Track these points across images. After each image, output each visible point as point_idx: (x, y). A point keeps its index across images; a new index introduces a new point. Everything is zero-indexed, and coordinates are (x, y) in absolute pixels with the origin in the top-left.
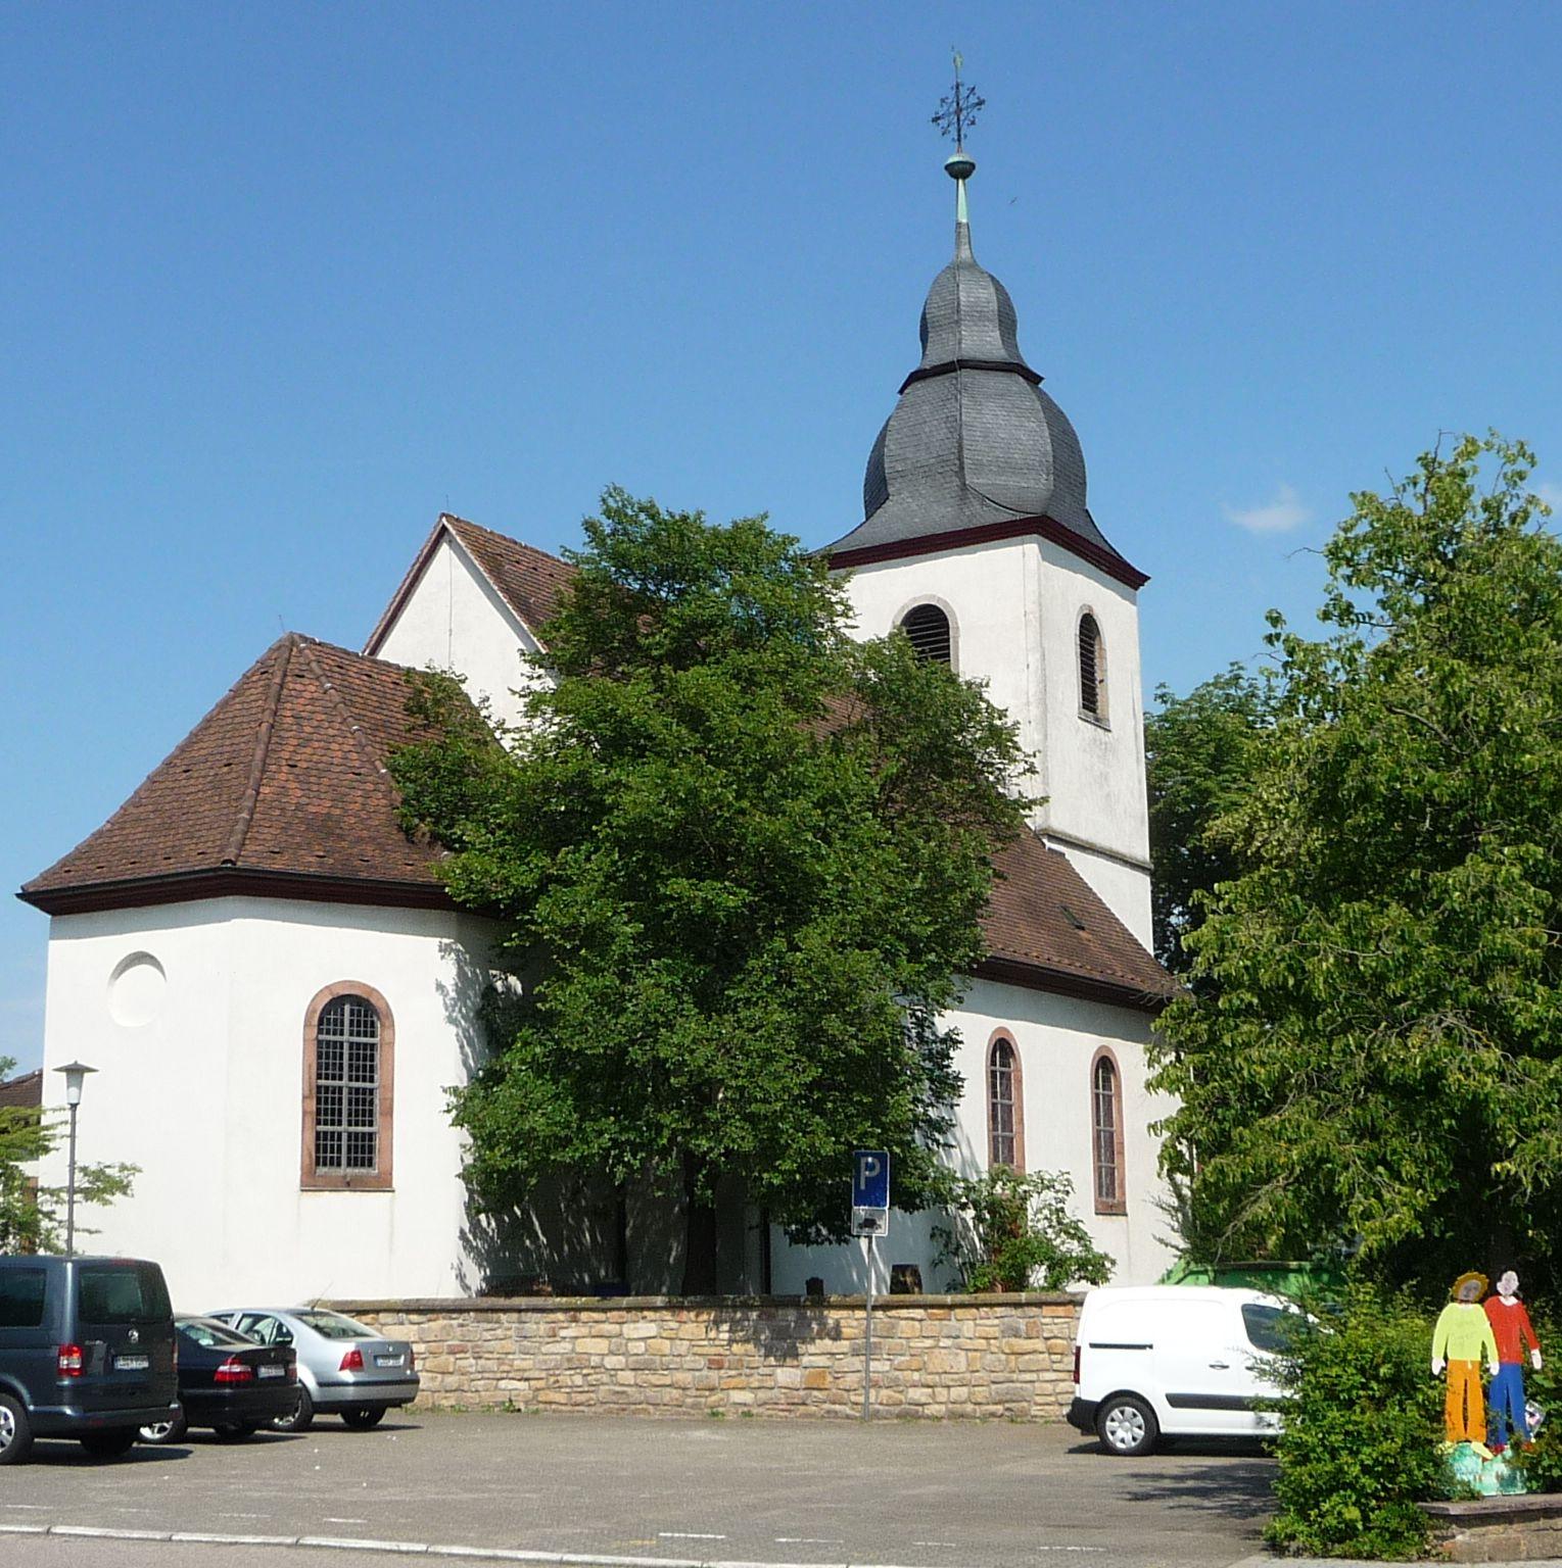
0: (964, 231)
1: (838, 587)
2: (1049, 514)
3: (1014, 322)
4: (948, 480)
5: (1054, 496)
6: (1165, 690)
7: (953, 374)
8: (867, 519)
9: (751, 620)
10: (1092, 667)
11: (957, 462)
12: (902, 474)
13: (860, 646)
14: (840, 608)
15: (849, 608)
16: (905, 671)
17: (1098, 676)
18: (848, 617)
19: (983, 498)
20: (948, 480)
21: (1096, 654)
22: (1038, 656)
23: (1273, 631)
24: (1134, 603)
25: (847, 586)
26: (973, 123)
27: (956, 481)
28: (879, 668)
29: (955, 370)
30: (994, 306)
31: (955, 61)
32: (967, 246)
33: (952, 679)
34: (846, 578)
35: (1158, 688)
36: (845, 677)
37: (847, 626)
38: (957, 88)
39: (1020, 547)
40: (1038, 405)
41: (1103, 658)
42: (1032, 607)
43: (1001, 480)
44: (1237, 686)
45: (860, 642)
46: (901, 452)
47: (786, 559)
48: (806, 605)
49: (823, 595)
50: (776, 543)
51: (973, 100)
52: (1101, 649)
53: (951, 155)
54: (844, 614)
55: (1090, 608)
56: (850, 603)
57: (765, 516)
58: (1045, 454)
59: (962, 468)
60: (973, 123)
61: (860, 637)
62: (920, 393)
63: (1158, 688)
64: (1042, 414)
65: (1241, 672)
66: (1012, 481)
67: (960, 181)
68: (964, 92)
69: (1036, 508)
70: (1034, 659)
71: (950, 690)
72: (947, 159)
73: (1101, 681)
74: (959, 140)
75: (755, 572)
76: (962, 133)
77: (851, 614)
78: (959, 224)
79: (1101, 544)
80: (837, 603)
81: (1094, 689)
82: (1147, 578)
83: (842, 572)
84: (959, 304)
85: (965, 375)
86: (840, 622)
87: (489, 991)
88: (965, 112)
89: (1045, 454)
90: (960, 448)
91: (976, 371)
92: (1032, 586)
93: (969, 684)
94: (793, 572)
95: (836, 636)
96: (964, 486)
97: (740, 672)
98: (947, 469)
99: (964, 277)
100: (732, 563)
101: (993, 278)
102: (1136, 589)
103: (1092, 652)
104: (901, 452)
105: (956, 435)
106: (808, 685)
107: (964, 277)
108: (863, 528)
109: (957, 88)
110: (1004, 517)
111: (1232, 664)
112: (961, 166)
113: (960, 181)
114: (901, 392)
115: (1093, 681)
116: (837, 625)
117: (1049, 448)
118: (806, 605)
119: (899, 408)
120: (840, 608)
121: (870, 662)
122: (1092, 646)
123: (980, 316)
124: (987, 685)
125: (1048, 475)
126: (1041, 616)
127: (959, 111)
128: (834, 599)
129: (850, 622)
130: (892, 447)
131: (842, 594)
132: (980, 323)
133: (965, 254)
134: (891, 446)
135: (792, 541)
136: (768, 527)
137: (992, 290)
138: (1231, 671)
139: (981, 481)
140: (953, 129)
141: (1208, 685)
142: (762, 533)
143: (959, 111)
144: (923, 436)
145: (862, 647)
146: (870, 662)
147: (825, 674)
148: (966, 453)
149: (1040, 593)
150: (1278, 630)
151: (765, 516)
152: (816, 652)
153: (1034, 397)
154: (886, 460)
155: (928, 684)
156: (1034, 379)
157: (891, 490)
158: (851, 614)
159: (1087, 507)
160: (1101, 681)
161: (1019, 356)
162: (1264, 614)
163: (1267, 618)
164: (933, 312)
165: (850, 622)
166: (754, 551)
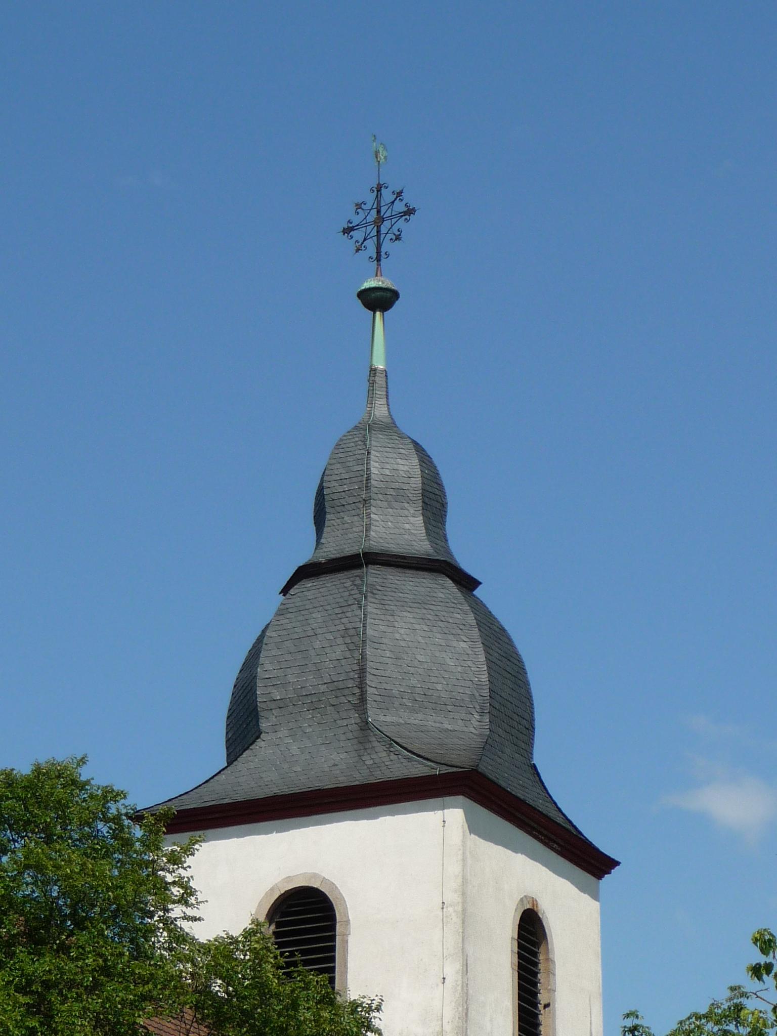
0: (380, 380)
1: (175, 860)
2: (482, 768)
3: (444, 505)
4: (344, 715)
5: (488, 745)
6: (636, 1022)
7: (357, 572)
8: (230, 763)
9: (51, 905)
10: (535, 984)
11: (357, 691)
12: (281, 705)
13: (202, 945)
14: (176, 891)
15: (189, 892)
16: (261, 987)
17: (543, 998)
18: (187, 904)
19: (391, 742)
20: (344, 715)
21: (541, 966)
22: (458, 966)
23: (762, 959)
24: (595, 896)
25: (189, 861)
26: (398, 238)
27: (355, 717)
28: (228, 980)
29: (359, 566)
30: (417, 482)
31: (377, 154)
32: (384, 401)
33: (328, 999)
34: (188, 850)
35: (628, 1016)
36: (179, 989)
37: (186, 918)
38: (379, 190)
39: (440, 812)
40: (471, 618)
41: (550, 973)
42: (452, 897)
43: (416, 719)
44: (738, 1021)
45: (203, 940)
46: (280, 673)
47: (106, 820)
48: (130, 888)
49: (154, 873)
50: (92, 796)
51: (399, 207)
52: (548, 960)
53: (365, 280)
54: (183, 900)
55: (534, 902)
56: (192, 884)
57: (83, 761)
58: (479, 686)
59: (363, 699)
60: (398, 238)
61: (203, 933)
62: (310, 595)
63: (628, 1016)
64: (476, 631)
65: (743, 1000)
66: (432, 721)
67: (378, 314)
68: (387, 196)
69: (463, 759)
70: (452, 970)
71: (326, 1014)
72: (362, 284)
73: (547, 1006)
74: (378, 259)
75: (60, 837)
76: (383, 250)
77: (192, 900)
78: (373, 371)
79: (553, 814)
80: (174, 883)
81: (536, 1016)
82: (617, 863)
83: (184, 838)
84: (368, 479)
85: (373, 575)
86: (177, 911)
87: (534, 928)
88: (387, 224)
89: (479, 686)
90: (362, 671)
91: (390, 570)
92: (454, 868)
93: (355, 1006)
94: (114, 837)
95: (170, 931)
96: (365, 726)
97: (30, 983)
98: (343, 699)
99: (377, 441)
100: (28, 822)
101: (416, 445)
102: (600, 877)
103: (536, 964)
104: (280, 673)
105: (357, 655)
106: (123, 1002)
107: (377, 441)
108: (222, 777)
109: (379, 190)
110: (419, 769)
111: (732, 989)
112: (379, 294)
113: (378, 314)
114: (285, 591)
115: (535, 1005)
116: (172, 915)
117: (485, 678)
118: (130, 888)
119: (281, 612)
120: (176, 891)
121: (215, 970)
122: (535, 954)
123: (399, 496)
124: (378, 1009)
125: (482, 714)
126: (464, 910)
127: (380, 220)
128: (169, 878)
129: (190, 912)
130: (268, 667)
131: (181, 871)
132: (395, 504)
133: (380, 410)
134: (267, 667)
135: (121, 795)
136: (84, 774)
137: (415, 461)
138: (731, 999)
139: (389, 719)
140: (371, 244)
141: (698, 1017)
142: (74, 782)
143: (380, 220)
144: (312, 653)
145: (205, 949)
146: (215, 970)
147: (150, 986)
148: (370, 680)
149: (464, 877)
150: (769, 959)
151: (83, 761)
152: (139, 954)
153: (466, 607)
154: (259, 684)
155: (295, 1006)
156: (467, 583)
157: (264, 725)
158: (192, 900)
159: (536, 761)
160: (547, 1006)
161: (448, 552)
162: (752, 930)
163: (756, 941)
164: (333, 486)
165: (190, 912)
166: (61, 806)
